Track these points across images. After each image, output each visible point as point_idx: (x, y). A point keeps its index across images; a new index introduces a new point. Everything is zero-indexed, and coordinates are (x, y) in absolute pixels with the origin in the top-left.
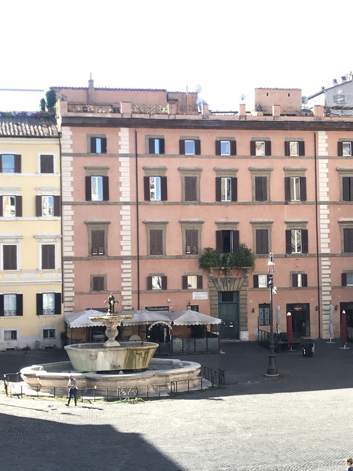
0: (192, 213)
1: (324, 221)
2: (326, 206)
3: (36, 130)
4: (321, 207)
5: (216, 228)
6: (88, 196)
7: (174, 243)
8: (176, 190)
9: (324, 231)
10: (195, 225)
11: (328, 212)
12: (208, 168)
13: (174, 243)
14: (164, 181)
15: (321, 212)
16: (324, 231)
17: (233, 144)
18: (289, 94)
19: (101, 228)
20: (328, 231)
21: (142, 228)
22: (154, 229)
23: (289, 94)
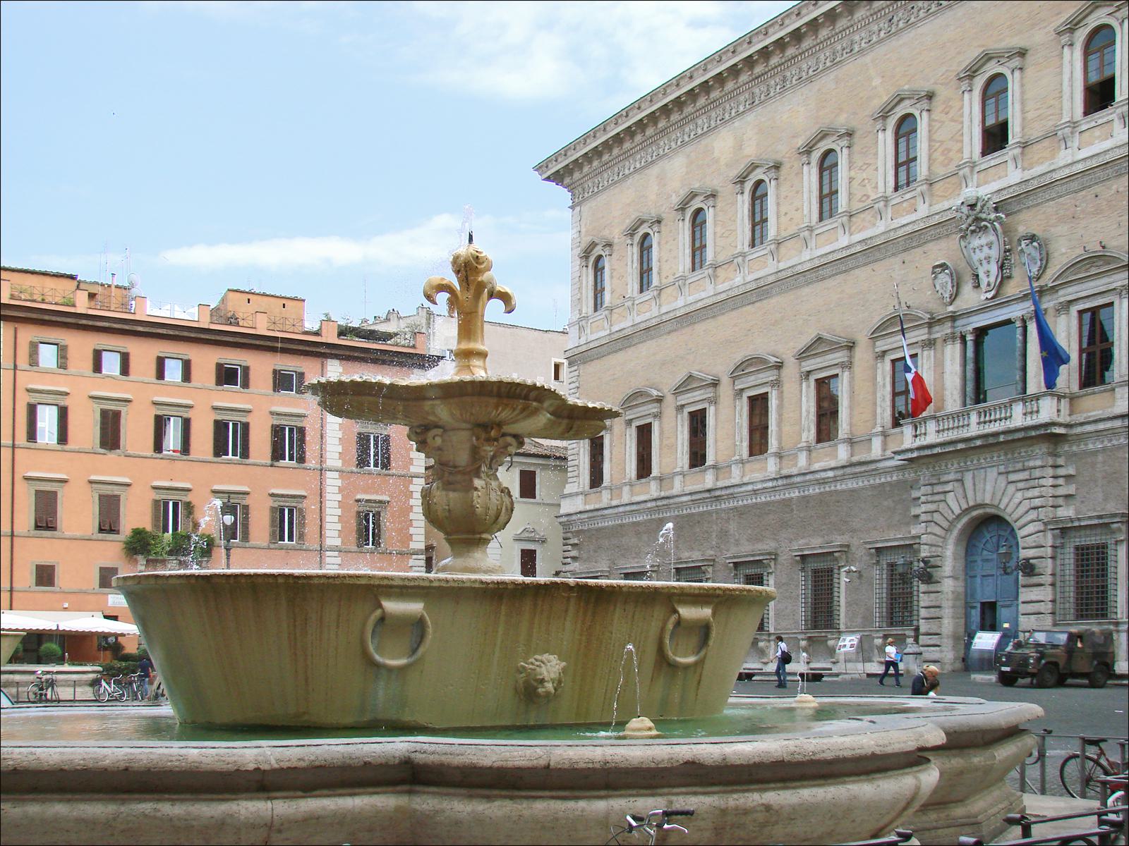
0: (111, 468)
1: (333, 497)
2: (336, 475)
3: (1042, 482)
4: (329, 474)
5: (271, 503)
6: (158, 447)
7: (77, 513)
8: (86, 428)
9: (333, 512)
10: (115, 487)
11: (339, 483)
12: (140, 397)
13: (77, 513)
14: (187, 424)
15: (329, 482)
16: (333, 512)
17: (125, 358)
18: (249, 300)
19: (116, 491)
20: (339, 512)
21: (21, 487)
22: (42, 488)
23: (249, 300)
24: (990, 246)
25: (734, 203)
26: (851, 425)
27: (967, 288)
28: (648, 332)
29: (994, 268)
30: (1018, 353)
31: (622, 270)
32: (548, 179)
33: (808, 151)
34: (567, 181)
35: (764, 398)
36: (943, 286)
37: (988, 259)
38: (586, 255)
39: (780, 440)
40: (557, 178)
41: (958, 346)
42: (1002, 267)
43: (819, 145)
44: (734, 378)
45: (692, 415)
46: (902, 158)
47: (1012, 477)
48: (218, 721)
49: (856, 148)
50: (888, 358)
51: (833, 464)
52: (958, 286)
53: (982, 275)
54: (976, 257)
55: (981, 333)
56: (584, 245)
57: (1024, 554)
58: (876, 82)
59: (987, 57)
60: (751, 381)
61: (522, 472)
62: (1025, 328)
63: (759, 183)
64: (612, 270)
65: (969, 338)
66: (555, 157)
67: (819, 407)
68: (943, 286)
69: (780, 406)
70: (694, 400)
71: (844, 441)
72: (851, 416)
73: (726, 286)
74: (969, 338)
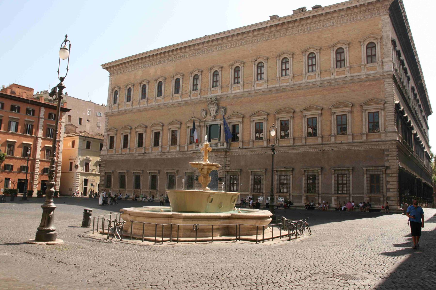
24: (214, 107)
25: (171, 82)
26: (180, 142)
27: (208, 115)
28: (129, 112)
29: (215, 113)
30: (219, 132)
31: (122, 96)
32: (104, 68)
33: (280, 56)
34: (109, 70)
35: (142, 134)
36: (203, 114)
37: (213, 110)
38: (113, 90)
39: (162, 143)
40: (107, 69)
41: (206, 128)
42: (216, 113)
43: (337, 45)
44: (151, 127)
45: (156, 133)
46: (236, 76)
47: (217, 159)
48: (409, 231)
49: (184, 79)
50: (255, 122)
51: (175, 151)
52: (206, 114)
53: (212, 114)
54: (211, 109)
55: (211, 126)
56: (112, 87)
57: (219, 176)
58: (190, 65)
59: (339, 43)
60: (155, 128)
61: (87, 142)
62: (220, 127)
63: (130, 88)
64: (120, 95)
65: (208, 127)
66: (107, 64)
67: (172, 137)
68: (203, 114)
69: (163, 136)
70: (141, 130)
71: (364, 134)
72: (180, 140)
73: (150, 104)
74: (208, 127)
